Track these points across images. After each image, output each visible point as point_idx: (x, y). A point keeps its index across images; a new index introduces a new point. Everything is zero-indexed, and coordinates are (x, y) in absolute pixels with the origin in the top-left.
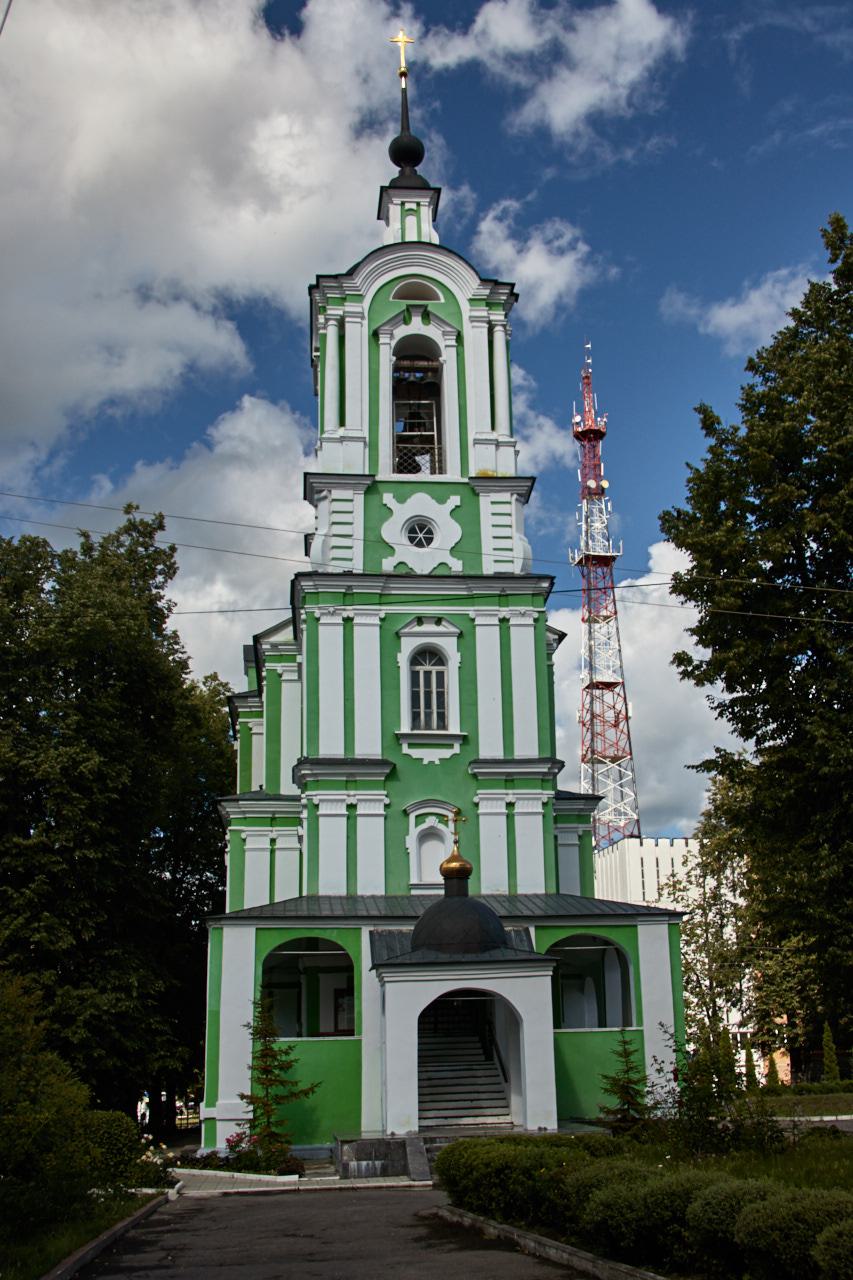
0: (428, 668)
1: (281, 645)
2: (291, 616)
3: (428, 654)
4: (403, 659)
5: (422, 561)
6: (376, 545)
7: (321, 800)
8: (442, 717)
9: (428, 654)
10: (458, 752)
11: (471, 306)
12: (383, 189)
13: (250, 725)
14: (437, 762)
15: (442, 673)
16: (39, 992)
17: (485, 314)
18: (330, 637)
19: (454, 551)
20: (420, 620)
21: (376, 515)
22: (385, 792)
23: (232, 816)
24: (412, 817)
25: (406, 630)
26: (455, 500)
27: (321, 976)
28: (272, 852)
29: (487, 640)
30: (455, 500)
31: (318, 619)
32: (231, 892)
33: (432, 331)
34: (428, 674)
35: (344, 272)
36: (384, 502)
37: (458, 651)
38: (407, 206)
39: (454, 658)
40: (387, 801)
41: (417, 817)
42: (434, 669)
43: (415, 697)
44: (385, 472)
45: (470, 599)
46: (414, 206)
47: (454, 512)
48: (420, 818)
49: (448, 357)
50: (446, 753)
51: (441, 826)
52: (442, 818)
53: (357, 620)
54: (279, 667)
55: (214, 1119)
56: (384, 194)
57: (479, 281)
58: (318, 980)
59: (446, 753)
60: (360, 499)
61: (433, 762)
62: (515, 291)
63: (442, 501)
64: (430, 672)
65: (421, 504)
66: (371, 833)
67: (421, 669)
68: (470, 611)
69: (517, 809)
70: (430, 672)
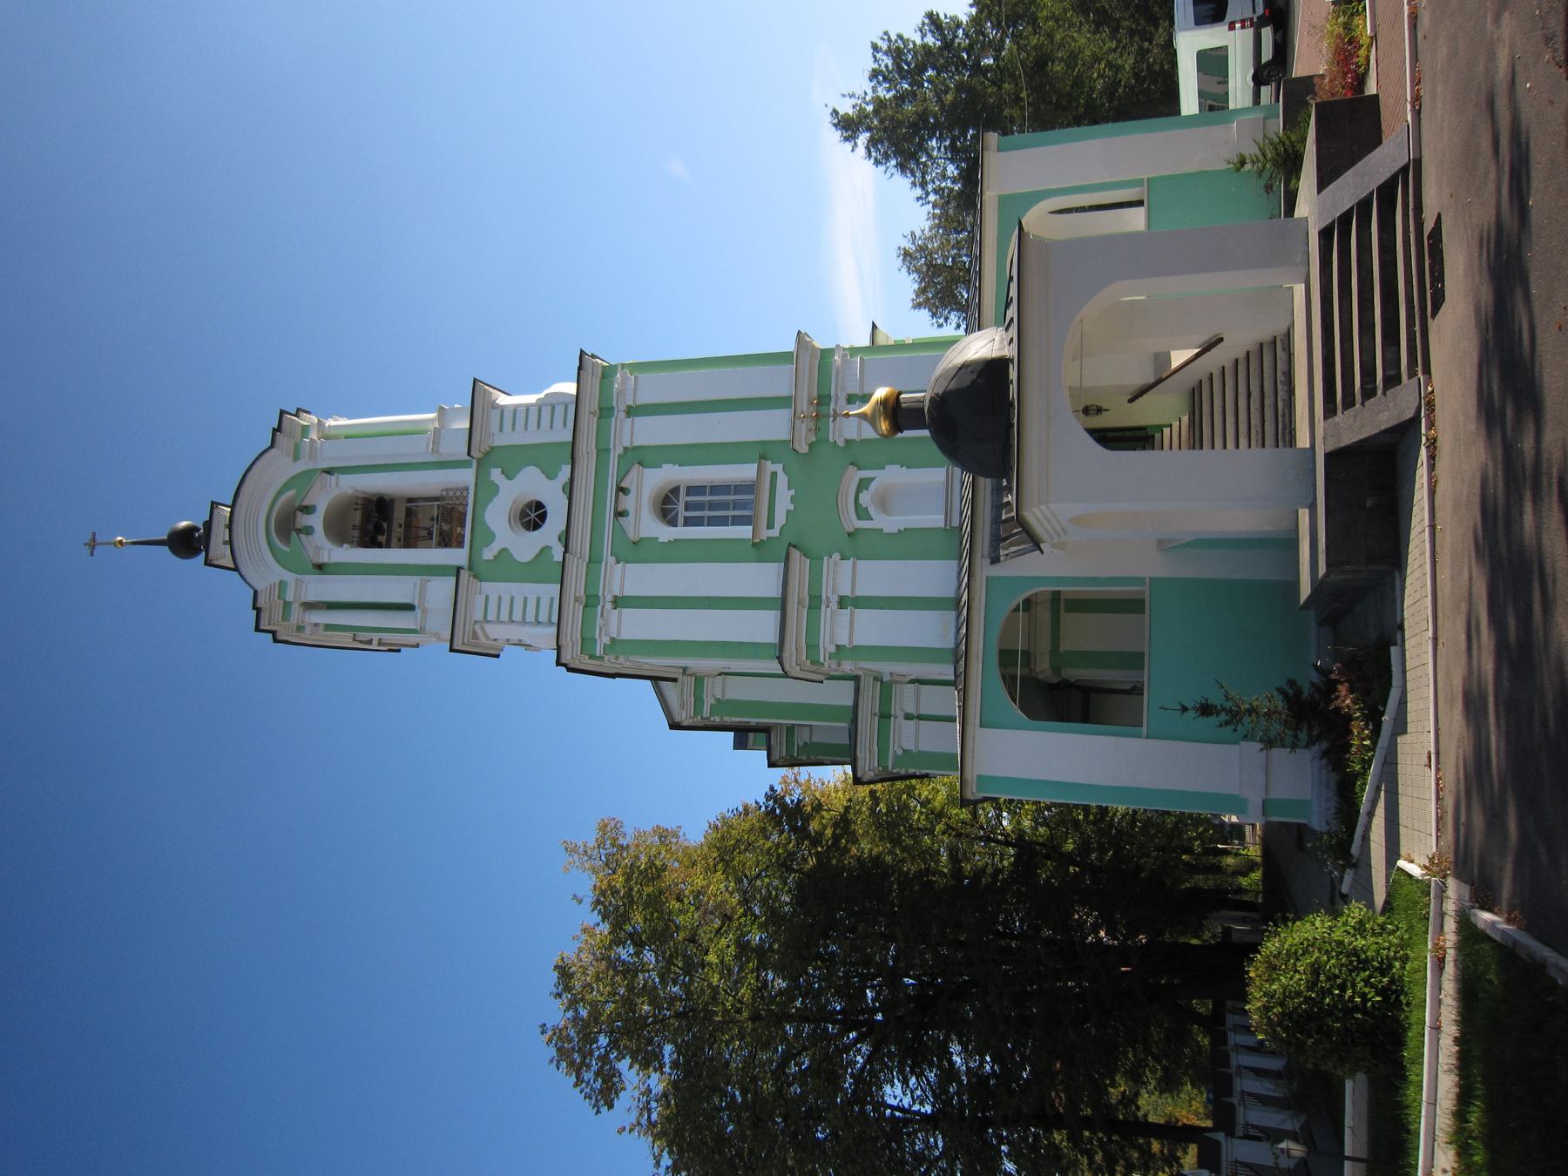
0: (681, 506)
1: (682, 698)
2: (649, 681)
3: (666, 507)
4: (666, 533)
5: (556, 507)
6: (533, 571)
7: (831, 641)
8: (740, 488)
9: (666, 507)
10: (781, 465)
13: (801, 744)
14: (792, 492)
15: (688, 488)
18: (638, 625)
19: (551, 476)
21: (505, 567)
22: (825, 558)
23: (784, 754)
26: (496, 475)
27: (1063, 648)
28: (921, 718)
29: (649, 431)
30: (496, 475)
31: (613, 639)
32: (756, 717)
34: (688, 507)
36: (492, 558)
40: (836, 556)
41: (859, 518)
42: (683, 498)
43: (713, 522)
44: (456, 556)
45: (602, 452)
47: (509, 475)
48: (862, 513)
50: (782, 480)
51: (873, 486)
52: (863, 484)
53: (617, 593)
54: (708, 702)
55: (1264, 802)
56: (215, 563)
58: (1065, 652)
60: (487, 586)
61: (792, 497)
63: (495, 489)
65: (498, 516)
66: (876, 577)
67: (682, 514)
68: (616, 451)
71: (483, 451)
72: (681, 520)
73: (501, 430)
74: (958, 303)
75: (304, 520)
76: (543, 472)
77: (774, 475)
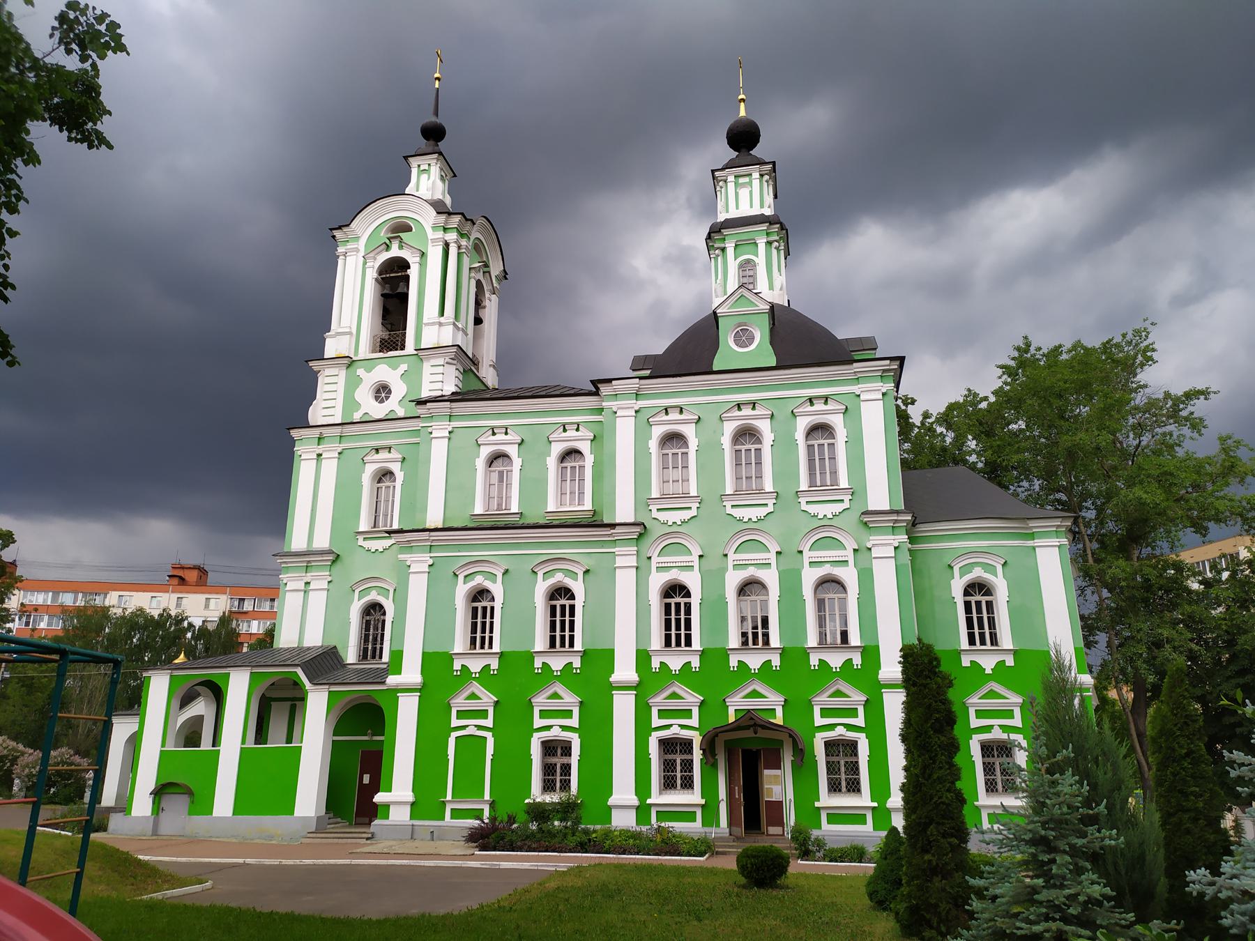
0: (978, 598)
11: (433, 231)
17: (441, 236)
20: (739, 406)
24: (461, 578)
25: (801, 410)
30: (404, 367)
33: (405, 254)
34: (563, 607)
37: (696, 437)
38: (422, 168)
39: (589, 460)
46: (426, 167)
49: (413, 273)
57: (436, 213)
59: (838, 508)
64: (980, 602)
66: (318, 601)
67: (973, 599)
69: (312, 586)
70: (980, 602)
72: (968, 598)
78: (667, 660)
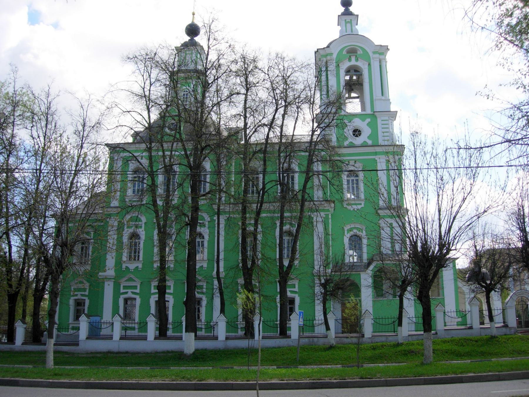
0: (353, 178)
5: (358, 141)
12: (339, 16)
16: (187, 219)
26: (368, 120)
30: (368, 120)
33: (359, 64)
34: (353, 180)
35: (326, 47)
42: (355, 178)
47: (368, 124)
62: (193, 334)
63: (363, 120)
67: (351, 179)
71: (505, 137)
72: (348, 178)
73: (382, 120)
74: (17, 221)
75: (353, 58)
76: (370, 135)
77: (361, 204)
78: (128, 265)
